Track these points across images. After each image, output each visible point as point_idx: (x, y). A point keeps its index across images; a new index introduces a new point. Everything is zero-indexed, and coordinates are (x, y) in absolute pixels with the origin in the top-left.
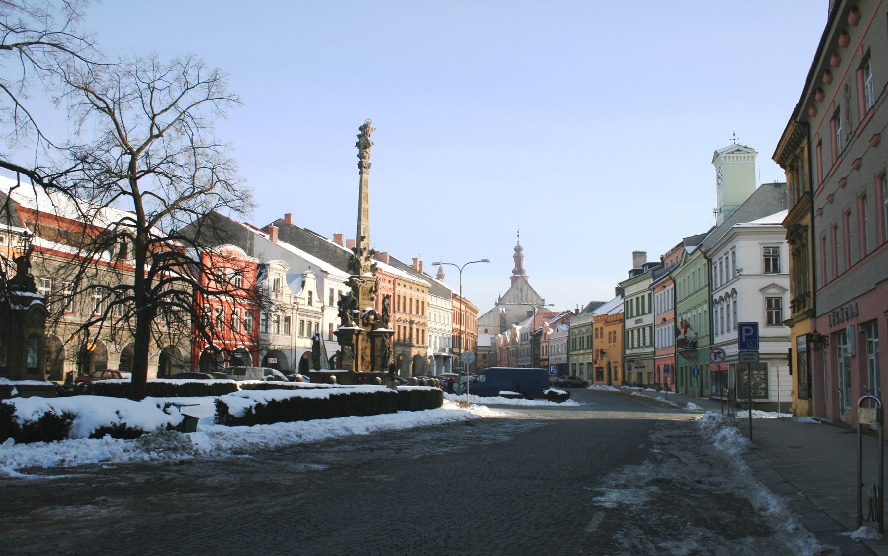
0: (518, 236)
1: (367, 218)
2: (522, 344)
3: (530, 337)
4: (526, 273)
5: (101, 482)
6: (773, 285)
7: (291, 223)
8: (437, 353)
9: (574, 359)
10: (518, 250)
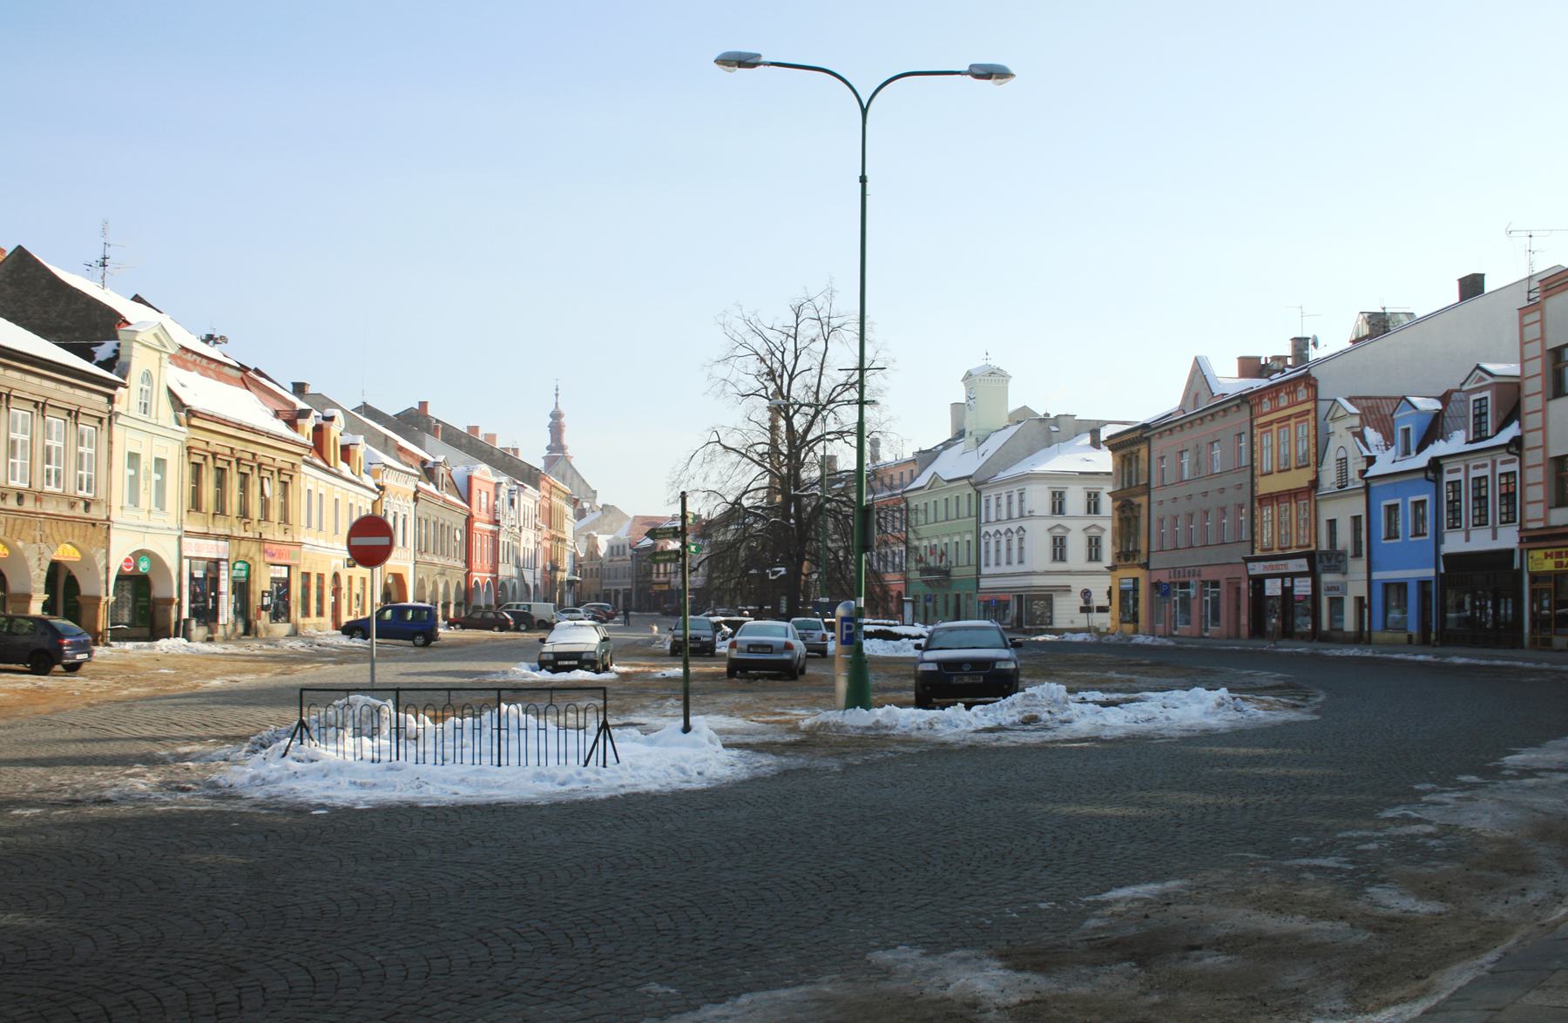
0: (557, 395)
2: (611, 561)
3: (629, 552)
4: (567, 451)
5: (588, 781)
6: (1059, 526)
7: (429, 414)
10: (556, 416)
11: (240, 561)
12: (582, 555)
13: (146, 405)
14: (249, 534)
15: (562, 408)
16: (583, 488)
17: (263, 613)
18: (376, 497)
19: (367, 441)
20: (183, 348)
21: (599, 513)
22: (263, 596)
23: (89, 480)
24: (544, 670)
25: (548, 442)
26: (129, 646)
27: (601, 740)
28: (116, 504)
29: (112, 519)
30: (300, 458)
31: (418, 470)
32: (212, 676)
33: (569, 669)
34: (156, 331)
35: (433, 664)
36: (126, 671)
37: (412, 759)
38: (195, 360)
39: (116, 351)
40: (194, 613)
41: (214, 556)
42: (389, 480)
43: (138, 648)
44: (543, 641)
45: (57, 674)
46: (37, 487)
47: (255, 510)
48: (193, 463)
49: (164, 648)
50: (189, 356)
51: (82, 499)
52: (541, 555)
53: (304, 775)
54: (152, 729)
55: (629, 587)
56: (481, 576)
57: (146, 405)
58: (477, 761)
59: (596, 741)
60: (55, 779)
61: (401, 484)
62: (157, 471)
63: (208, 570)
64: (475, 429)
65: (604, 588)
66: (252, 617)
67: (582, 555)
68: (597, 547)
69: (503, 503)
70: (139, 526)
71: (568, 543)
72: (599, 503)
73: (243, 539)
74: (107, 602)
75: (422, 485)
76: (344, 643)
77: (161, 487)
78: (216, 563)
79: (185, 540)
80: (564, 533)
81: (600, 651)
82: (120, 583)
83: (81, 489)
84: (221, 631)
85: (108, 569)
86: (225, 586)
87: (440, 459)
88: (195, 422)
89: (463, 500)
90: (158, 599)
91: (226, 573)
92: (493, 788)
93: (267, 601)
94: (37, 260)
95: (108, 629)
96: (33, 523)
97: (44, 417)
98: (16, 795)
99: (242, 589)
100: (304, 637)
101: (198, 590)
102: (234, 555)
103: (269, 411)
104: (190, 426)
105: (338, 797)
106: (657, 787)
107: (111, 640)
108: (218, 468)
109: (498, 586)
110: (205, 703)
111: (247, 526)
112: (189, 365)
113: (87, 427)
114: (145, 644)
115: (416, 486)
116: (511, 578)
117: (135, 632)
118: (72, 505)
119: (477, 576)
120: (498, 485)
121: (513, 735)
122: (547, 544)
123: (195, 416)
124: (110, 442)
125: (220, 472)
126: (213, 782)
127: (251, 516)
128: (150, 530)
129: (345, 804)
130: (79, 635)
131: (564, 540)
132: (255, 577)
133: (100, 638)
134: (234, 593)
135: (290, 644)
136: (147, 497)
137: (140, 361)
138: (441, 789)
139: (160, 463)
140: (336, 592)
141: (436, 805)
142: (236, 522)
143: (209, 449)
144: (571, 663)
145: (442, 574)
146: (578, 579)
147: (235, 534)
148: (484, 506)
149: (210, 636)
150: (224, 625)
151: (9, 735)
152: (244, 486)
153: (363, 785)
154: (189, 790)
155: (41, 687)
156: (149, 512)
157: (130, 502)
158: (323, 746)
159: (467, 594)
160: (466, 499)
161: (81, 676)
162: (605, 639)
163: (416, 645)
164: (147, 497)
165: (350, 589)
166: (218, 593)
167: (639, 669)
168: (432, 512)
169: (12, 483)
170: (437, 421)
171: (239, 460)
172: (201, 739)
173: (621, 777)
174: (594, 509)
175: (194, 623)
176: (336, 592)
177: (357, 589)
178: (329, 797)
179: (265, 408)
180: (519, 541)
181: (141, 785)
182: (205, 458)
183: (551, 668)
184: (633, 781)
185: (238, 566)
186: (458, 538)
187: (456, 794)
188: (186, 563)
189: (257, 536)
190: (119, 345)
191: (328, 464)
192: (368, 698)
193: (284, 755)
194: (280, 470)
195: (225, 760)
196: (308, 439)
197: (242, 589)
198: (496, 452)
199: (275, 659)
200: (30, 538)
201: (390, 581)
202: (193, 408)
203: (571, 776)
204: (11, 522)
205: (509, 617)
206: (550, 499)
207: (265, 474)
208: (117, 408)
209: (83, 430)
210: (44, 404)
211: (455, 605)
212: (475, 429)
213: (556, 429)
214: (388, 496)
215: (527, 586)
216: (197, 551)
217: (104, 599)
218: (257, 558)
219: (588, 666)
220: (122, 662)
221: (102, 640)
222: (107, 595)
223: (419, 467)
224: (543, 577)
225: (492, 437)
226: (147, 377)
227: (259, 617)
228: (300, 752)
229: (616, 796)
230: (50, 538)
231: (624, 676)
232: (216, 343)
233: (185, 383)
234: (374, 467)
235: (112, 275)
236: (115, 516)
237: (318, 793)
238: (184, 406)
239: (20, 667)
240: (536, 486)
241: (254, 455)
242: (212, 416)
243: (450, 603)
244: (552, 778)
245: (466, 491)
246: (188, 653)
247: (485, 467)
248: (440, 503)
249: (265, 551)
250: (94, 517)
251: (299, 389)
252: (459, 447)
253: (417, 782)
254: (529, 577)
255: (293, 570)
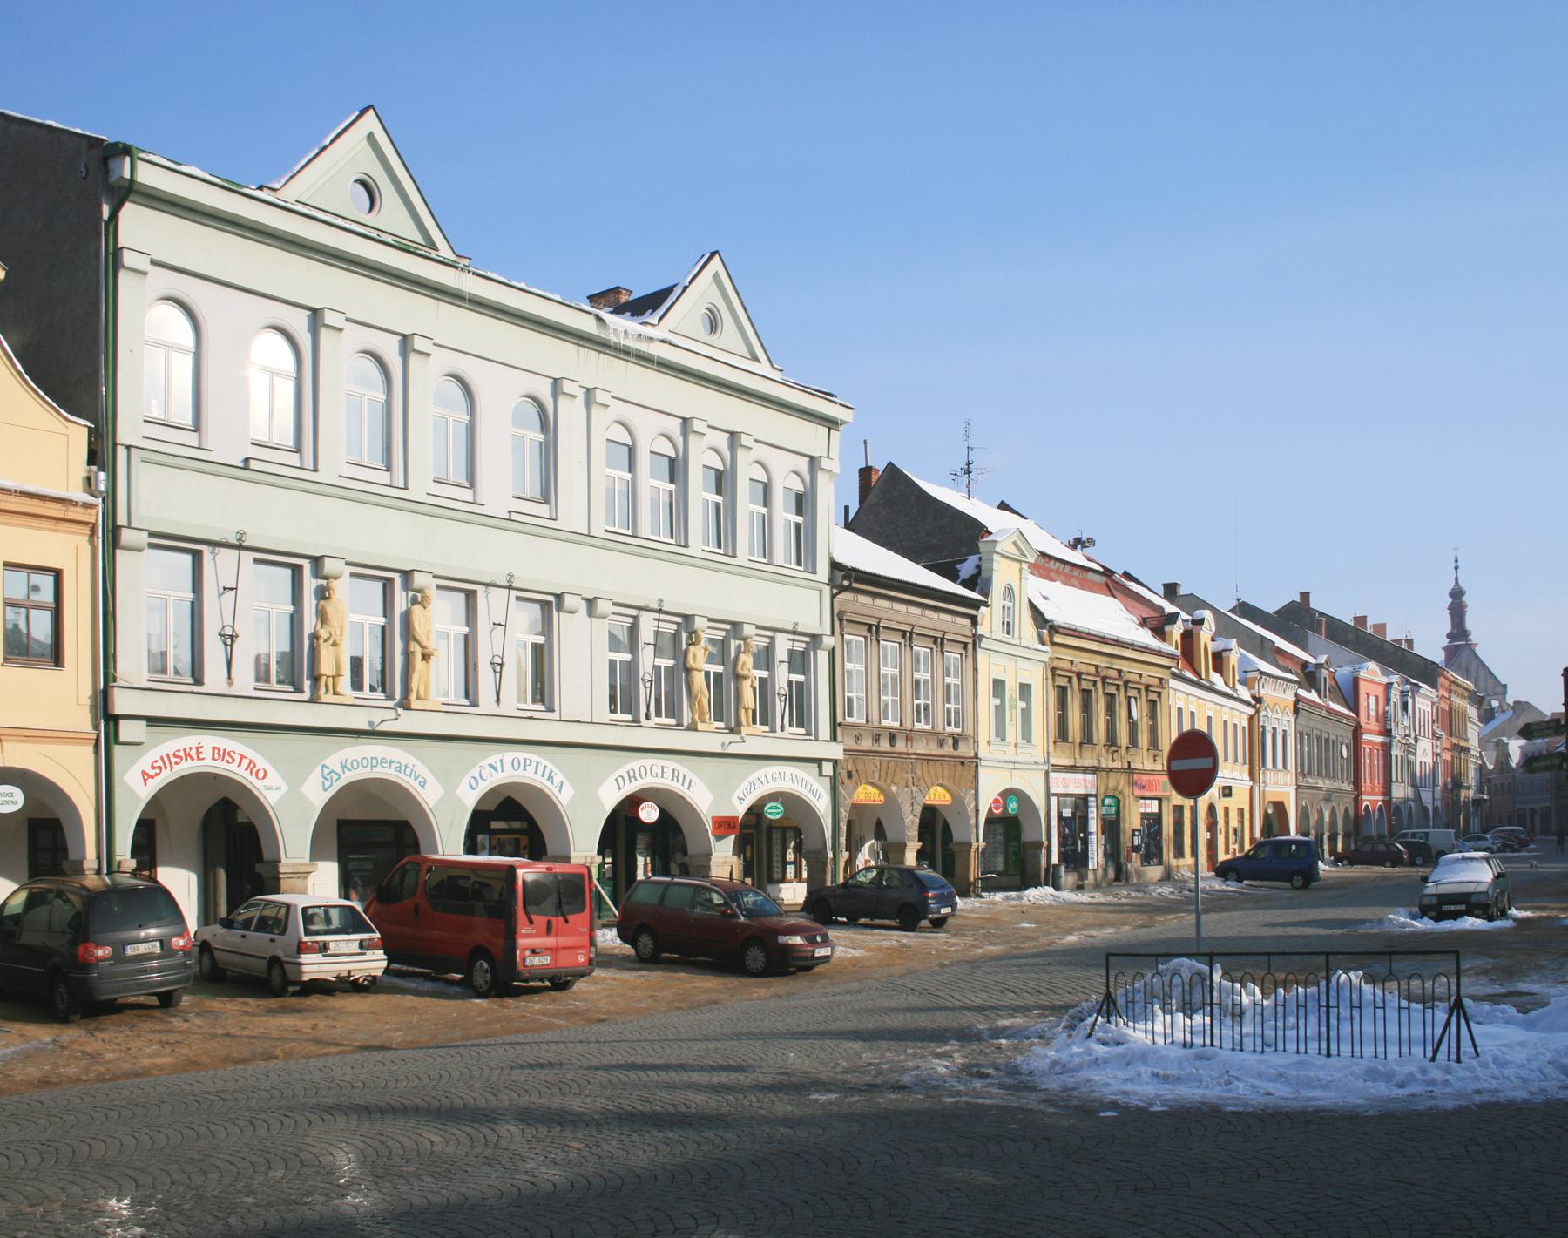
0: (1456, 568)
5: (1433, 1083)
10: (1457, 594)
11: (1109, 797)
12: (1491, 767)
13: (1008, 623)
14: (1117, 765)
15: (1462, 584)
16: (1490, 682)
17: (1134, 854)
18: (1251, 711)
19: (1241, 645)
20: (1043, 555)
21: (1510, 713)
22: (1134, 835)
23: (957, 713)
24: (1426, 919)
25: (1448, 628)
26: (999, 896)
27: (1454, 1019)
28: (983, 738)
29: (980, 756)
30: (1168, 672)
31: (1297, 675)
32: (1070, 932)
33: (1456, 915)
34: (1015, 538)
35: (1305, 911)
36: (989, 926)
37: (1227, 1045)
38: (1058, 569)
39: (978, 567)
40: (1063, 857)
41: (1082, 791)
42: (1267, 691)
43: (1008, 898)
44: (1425, 880)
45: (923, 930)
46: (908, 725)
47: (1123, 737)
48: (1058, 686)
49: (1031, 898)
50: (1052, 565)
51: (951, 735)
52: (1440, 770)
53: (1105, 1063)
54: (984, 995)
55: (1548, 804)
56: (1371, 800)
57: (1008, 623)
58: (1302, 1048)
59: (1448, 1024)
60: (867, 1057)
61: (1279, 694)
62: (1022, 699)
63: (1076, 808)
64: (1361, 620)
65: (1518, 807)
66: (1122, 860)
67: (1491, 767)
68: (1508, 755)
69: (1394, 709)
70: (1006, 762)
71: (1472, 752)
72: (1510, 699)
73: (1111, 770)
74: (978, 848)
75: (1302, 692)
76: (1217, 887)
77: (1026, 715)
78: (1084, 799)
79: (1052, 775)
80: (1467, 740)
81: (1494, 891)
82: (992, 827)
83: (949, 724)
84: (1091, 876)
85: (977, 811)
86: (1093, 826)
87: (1322, 659)
88: (1058, 639)
89: (1349, 708)
90: (1029, 843)
91: (1095, 810)
92: (1315, 1087)
93: (1137, 841)
94: (906, 476)
95: (978, 879)
96: (905, 766)
97: (912, 647)
98: (823, 1076)
99: (1112, 827)
100: (1176, 880)
101: (1067, 831)
102: (1102, 790)
103: (1135, 619)
104: (1053, 644)
105: (1136, 1093)
106: (1525, 1095)
107: (982, 891)
108: (1084, 690)
109: (1391, 809)
110: (1049, 964)
111: (1115, 755)
112: (1053, 574)
113: (952, 656)
114: (1014, 894)
115: (1296, 695)
116: (1406, 800)
117: (1006, 880)
118: (941, 743)
119: (1367, 801)
120: (1389, 686)
121: (1345, 1013)
122: (1447, 756)
123: (1057, 632)
124: (975, 670)
125: (1086, 694)
126: (1015, 1067)
127: (1118, 744)
128: (1017, 766)
129: (1141, 1104)
130: (943, 887)
131: (1467, 750)
132: (1125, 814)
133: (972, 889)
134: (1103, 833)
135: (1159, 890)
136: (1013, 730)
137: (1003, 573)
138: (1253, 1087)
139: (1025, 689)
140: (1212, 827)
141: (1241, 1109)
142: (1103, 751)
143: (1074, 669)
144: (1459, 907)
145: (1327, 799)
146: (1485, 797)
147: (1103, 765)
148: (1373, 713)
149: (1080, 883)
150: (1094, 870)
151: (850, 1002)
152: (1111, 709)
153: (1165, 1079)
154: (986, 1076)
155: (904, 945)
156: (1016, 745)
157: (997, 736)
158: (1131, 1024)
159: (1357, 822)
160: (1352, 706)
161: (946, 932)
162: (1498, 876)
163: (1294, 888)
164: (1013, 730)
165: (1227, 823)
166: (1087, 834)
167: (1544, 914)
168: (1317, 725)
169: (885, 723)
170: (1321, 614)
171: (1104, 679)
172: (1025, 1010)
173: (1477, 1079)
174: (1505, 708)
175: (1063, 868)
176: (1212, 827)
177: (1234, 823)
178: (1125, 1093)
179: (1130, 616)
180: (1415, 754)
181: (941, 1068)
182: (1070, 679)
183: (1433, 914)
184: (1494, 1084)
185: (1107, 801)
186: (1345, 755)
187: (1269, 1094)
188: (1054, 800)
189: (1126, 766)
190: (980, 559)
191: (1199, 676)
192: (1194, 962)
193: (1089, 1036)
194: (1147, 687)
195: (1041, 1038)
196: (1177, 648)
197: (1112, 827)
198: (1386, 646)
199: (1140, 908)
200: (903, 782)
201: (1270, 811)
202: (1056, 623)
203: (1411, 1074)
204: (885, 765)
205: (1402, 849)
206: (1449, 699)
207: (1132, 693)
208: (981, 630)
209: (949, 658)
210: (911, 633)
211: (1343, 837)
212: (1361, 620)
213: (1457, 610)
214: (1266, 710)
215: (1425, 809)
216: (1066, 786)
217: (975, 845)
218: (1126, 791)
219: (1479, 912)
220: (988, 916)
221: (974, 891)
222: (977, 840)
223: (1299, 671)
224: (1443, 797)
225: (1381, 628)
226: (1009, 592)
227: (1129, 860)
228: (1107, 1032)
229: (1468, 1107)
230: (922, 781)
231: (1522, 922)
232: (1084, 547)
233: (1048, 596)
234: (1250, 675)
235: (977, 482)
236: (983, 752)
237: (1116, 1086)
238: (1046, 621)
239: (892, 923)
240: (1433, 684)
241: (1120, 671)
242: (1075, 630)
243: (1337, 834)
244: (1388, 1077)
245: (1351, 693)
246: (1054, 903)
247: (1372, 666)
248: (1323, 713)
249: (1135, 784)
250: (962, 755)
251: (1171, 591)
252: (1345, 643)
253: (1226, 1077)
254: (1426, 797)
255: (1164, 804)
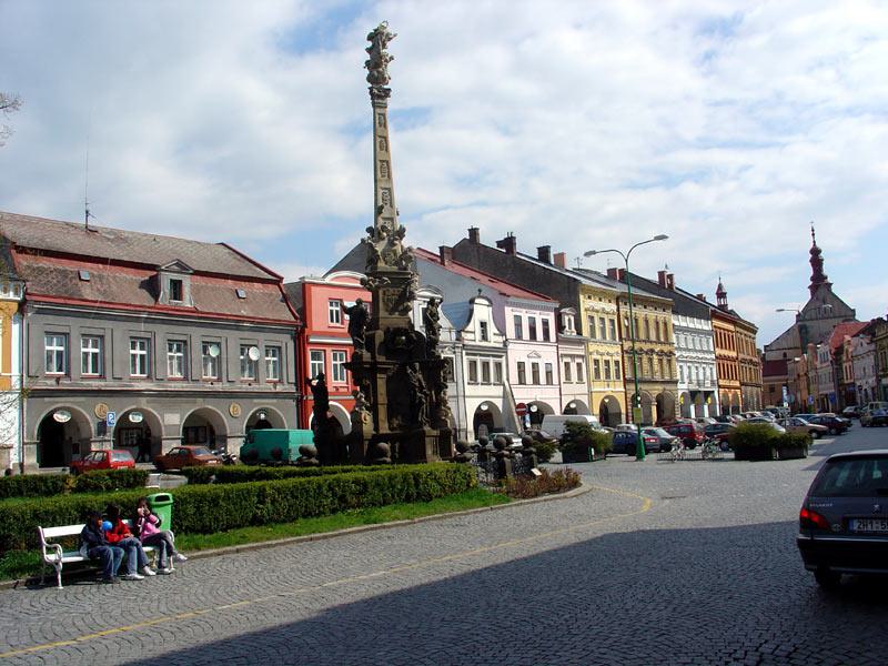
0: (813, 235)
1: (389, 176)
8: (694, 387)
9: (584, 388)
10: (815, 252)
